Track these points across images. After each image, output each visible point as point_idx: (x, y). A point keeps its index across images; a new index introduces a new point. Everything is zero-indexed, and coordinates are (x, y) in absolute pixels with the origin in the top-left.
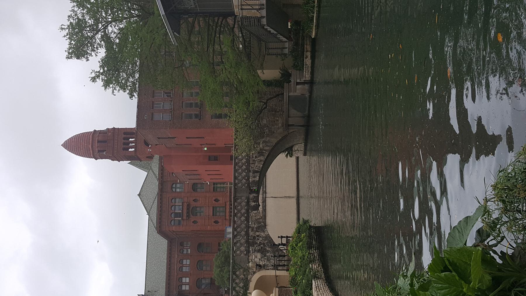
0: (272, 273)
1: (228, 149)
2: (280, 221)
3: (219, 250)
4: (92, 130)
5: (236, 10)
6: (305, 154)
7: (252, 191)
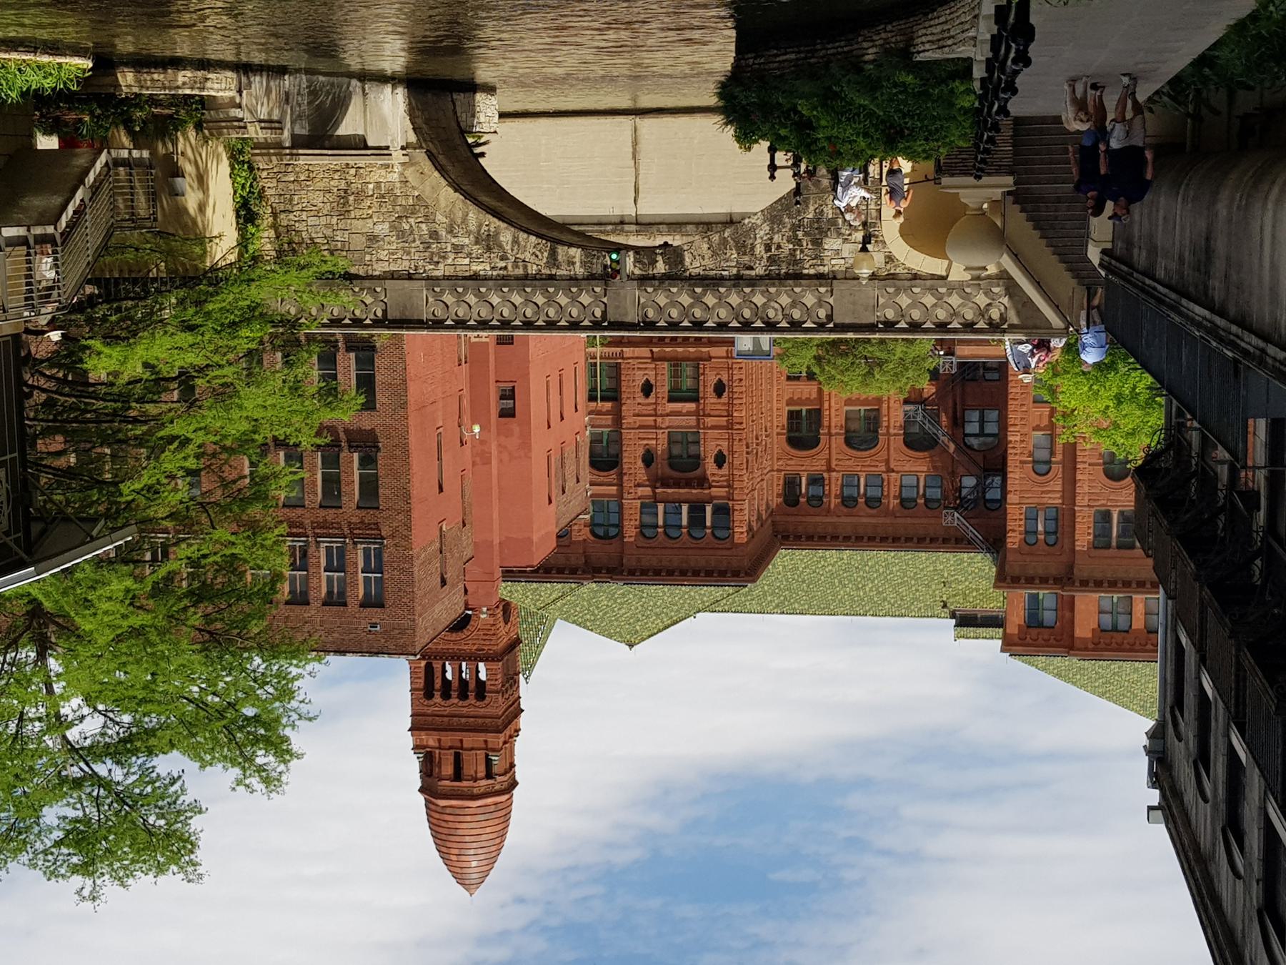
4: (421, 799)
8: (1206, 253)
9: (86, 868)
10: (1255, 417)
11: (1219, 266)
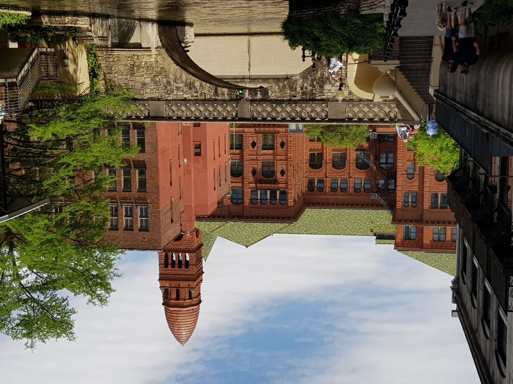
4: (163, 307)
9: (28, 335)
11: (481, 96)
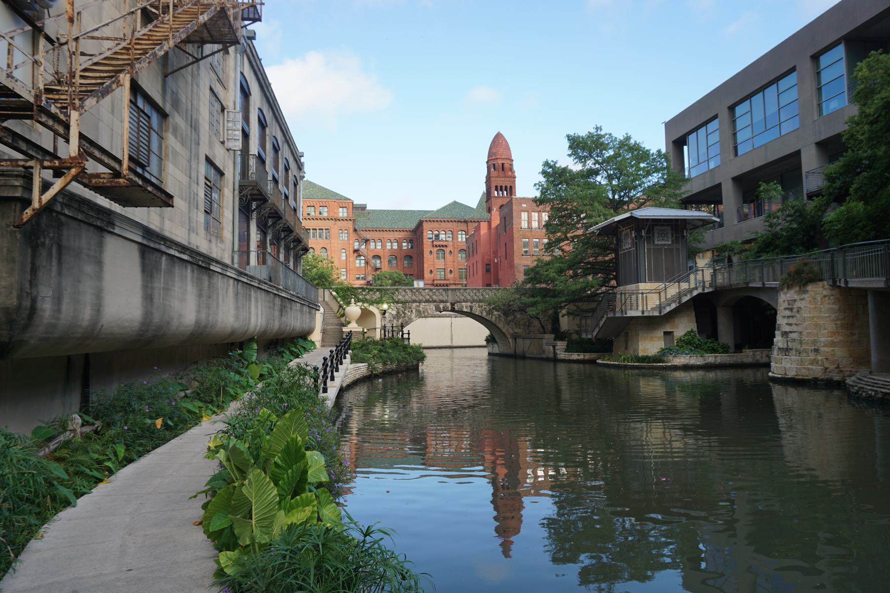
0: (378, 325)
1: (497, 281)
2: (423, 331)
3: (406, 275)
4: (513, 158)
5: (622, 288)
6: (489, 354)
7: (453, 304)
8: (282, 310)
9: (600, 137)
10: (360, 267)
11: (277, 308)
